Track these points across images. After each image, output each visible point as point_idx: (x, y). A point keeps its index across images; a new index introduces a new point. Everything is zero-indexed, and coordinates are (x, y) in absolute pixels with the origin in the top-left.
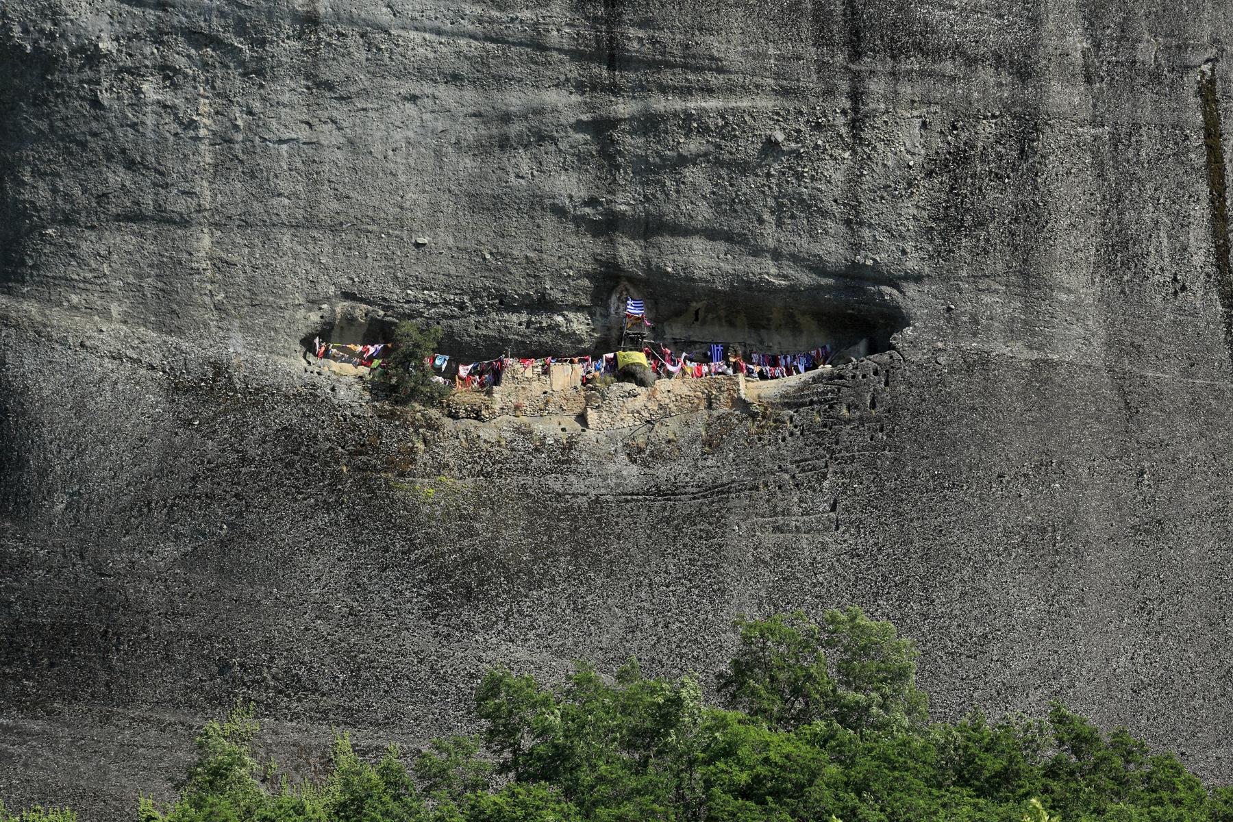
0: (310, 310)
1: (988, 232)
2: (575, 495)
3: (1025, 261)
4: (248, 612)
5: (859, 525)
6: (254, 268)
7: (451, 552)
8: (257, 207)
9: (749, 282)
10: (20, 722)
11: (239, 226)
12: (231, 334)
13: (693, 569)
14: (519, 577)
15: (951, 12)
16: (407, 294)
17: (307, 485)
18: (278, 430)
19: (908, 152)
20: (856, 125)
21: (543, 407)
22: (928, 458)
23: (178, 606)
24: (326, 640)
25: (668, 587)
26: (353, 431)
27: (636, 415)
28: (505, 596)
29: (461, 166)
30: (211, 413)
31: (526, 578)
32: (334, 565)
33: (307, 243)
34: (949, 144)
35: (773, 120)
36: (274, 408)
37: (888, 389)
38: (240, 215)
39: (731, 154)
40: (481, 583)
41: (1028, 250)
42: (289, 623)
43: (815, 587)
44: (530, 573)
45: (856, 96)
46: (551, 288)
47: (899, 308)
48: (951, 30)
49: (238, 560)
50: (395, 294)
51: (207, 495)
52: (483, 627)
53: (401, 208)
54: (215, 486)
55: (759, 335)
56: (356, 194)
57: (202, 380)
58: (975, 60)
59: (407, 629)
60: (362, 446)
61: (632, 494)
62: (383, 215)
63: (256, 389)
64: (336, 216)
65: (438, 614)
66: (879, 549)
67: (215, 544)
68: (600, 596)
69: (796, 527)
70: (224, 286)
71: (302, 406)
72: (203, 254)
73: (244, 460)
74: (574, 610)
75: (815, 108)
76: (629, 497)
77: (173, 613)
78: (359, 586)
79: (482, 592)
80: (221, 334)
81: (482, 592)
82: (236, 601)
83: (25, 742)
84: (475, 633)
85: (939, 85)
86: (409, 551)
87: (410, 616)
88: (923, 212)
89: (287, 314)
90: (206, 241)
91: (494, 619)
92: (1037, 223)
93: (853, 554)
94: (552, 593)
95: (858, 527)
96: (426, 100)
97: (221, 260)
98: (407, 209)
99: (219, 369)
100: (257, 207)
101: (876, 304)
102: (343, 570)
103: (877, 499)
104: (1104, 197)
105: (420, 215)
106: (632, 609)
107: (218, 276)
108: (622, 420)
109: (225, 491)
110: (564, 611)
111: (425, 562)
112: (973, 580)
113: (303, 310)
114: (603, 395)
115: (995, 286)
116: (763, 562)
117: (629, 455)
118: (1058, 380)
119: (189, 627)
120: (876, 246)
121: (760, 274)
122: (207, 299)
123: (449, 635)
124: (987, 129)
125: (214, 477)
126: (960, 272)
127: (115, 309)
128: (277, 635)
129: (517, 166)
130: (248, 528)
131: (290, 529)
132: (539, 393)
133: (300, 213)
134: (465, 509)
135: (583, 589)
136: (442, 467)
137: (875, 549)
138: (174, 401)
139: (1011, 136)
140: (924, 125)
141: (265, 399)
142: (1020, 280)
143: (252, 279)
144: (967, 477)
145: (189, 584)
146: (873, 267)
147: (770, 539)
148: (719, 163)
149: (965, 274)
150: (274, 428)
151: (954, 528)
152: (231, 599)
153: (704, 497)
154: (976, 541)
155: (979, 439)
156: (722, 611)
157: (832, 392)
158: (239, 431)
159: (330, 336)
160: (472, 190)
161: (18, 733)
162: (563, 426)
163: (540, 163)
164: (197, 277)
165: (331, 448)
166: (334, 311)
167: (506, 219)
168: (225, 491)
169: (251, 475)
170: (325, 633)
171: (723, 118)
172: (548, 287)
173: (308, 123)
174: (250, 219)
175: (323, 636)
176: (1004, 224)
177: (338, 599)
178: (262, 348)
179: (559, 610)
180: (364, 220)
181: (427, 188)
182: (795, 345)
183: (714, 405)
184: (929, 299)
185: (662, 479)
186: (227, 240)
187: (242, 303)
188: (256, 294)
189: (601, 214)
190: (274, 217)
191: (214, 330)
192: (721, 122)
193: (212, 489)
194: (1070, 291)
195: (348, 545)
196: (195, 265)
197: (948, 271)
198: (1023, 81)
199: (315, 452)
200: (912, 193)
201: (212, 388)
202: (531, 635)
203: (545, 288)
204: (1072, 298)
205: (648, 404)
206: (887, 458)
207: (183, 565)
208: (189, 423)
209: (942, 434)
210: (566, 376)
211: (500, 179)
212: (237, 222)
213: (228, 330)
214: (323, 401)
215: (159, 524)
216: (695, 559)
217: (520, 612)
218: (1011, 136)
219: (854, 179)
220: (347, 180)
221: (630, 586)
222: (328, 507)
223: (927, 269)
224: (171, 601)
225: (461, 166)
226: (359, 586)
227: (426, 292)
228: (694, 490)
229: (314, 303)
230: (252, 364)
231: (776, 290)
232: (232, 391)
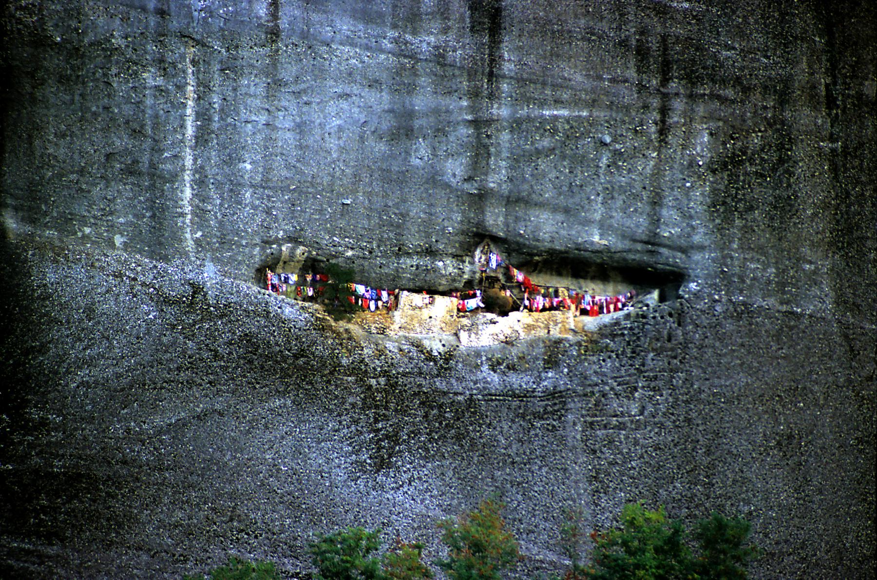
2: (456, 394)
10: (39, 548)
15: (733, 52)
16: (334, 241)
28: (408, 466)
30: (191, 321)
45: (664, 111)
48: (733, 66)
54: (194, 375)
55: (579, 283)
57: (184, 296)
58: (749, 89)
63: (225, 305)
73: (216, 356)
75: (634, 119)
76: (494, 398)
83: (43, 563)
85: (723, 107)
93: (657, 448)
96: (354, 98)
99: (197, 289)
101: (668, 265)
104: (837, 196)
112: (742, 472)
118: (802, 327)
124: (756, 140)
127: (118, 240)
133: (259, 178)
137: (672, 444)
138: (162, 310)
141: (231, 312)
146: (669, 238)
150: (238, 334)
153: (548, 400)
161: (37, 556)
162: (443, 342)
165: (280, 351)
171: (568, 123)
173: (267, 110)
189: (476, 189)
191: (193, 259)
192: (567, 127)
194: (811, 263)
202: (427, 496)
203: (432, 241)
204: (813, 267)
206: (680, 378)
210: (444, 305)
215: (151, 402)
217: (420, 479)
227: (347, 240)
228: (540, 394)
230: (221, 286)
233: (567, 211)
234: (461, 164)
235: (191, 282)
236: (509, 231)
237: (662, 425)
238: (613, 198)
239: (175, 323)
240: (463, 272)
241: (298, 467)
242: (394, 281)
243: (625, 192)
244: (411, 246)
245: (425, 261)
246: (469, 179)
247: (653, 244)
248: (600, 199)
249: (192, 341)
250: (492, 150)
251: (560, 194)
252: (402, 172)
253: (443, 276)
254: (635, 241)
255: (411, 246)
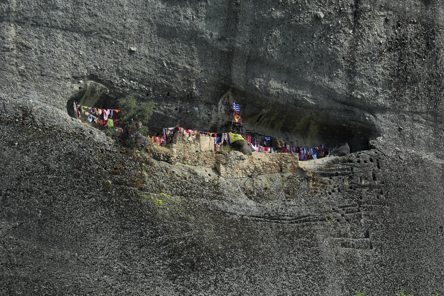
0: (73, 82)
1: (418, 87)
3: (435, 106)
4: (61, 267)
5: (381, 246)
6: (42, 52)
7: (180, 240)
8: (44, 14)
9: (296, 100)
11: (32, 25)
12: (30, 91)
13: (307, 264)
14: (219, 259)
16: (123, 81)
17: (90, 189)
18: (66, 154)
19: (378, 35)
20: (356, 15)
21: (196, 160)
22: (406, 212)
23: (14, 260)
24: (111, 288)
25: (296, 273)
26: (108, 159)
27: (244, 171)
29: (157, 6)
31: (223, 260)
32: (111, 242)
33: (72, 41)
34: (396, 34)
35: (318, 5)
36: (62, 140)
37: (380, 170)
38: (33, 18)
39: (296, 21)
40: (198, 260)
41: (437, 101)
42: (88, 275)
43: (367, 281)
44: (224, 257)
46: (196, 89)
47: (374, 125)
49: (51, 233)
50: (117, 80)
51: (27, 190)
52: (203, 288)
53: (124, 27)
54: (32, 185)
56: (101, 14)
57: (16, 118)
59: (159, 285)
60: (115, 169)
61: (257, 217)
62: (114, 30)
64: (89, 26)
65: (176, 278)
66: (392, 263)
67: (35, 222)
68: (262, 275)
69: (353, 245)
70: (25, 60)
71: (77, 140)
72: (10, 39)
73: (48, 170)
74: (250, 282)
77: (11, 264)
78: (127, 256)
79: (200, 266)
80: (24, 90)
81: (200, 266)
82: (52, 259)
84: (199, 291)
86: (155, 237)
87: (159, 277)
88: (387, 71)
89: (62, 83)
90: (13, 32)
91: (209, 283)
92: (440, 85)
94: (238, 270)
95: (381, 248)
97: (22, 44)
98: (127, 28)
100: (44, 14)
101: (360, 122)
102: (115, 245)
103: (387, 233)
105: (133, 33)
106: (280, 285)
107: (21, 54)
108: (237, 173)
109: (39, 189)
110: (245, 282)
111: (165, 244)
113: (70, 82)
114: (226, 156)
115: (421, 119)
116: (341, 263)
117: (246, 194)
119: (23, 274)
120: (362, 88)
121: (303, 96)
122: (14, 68)
123: (184, 291)
125: (31, 179)
126: (405, 108)
128: (81, 283)
129: (185, 11)
130: (56, 213)
131: (83, 216)
132: (194, 151)
133: (68, 21)
134: (181, 214)
135: (253, 270)
136: (160, 188)
137: (390, 262)
139: (421, 35)
140: (386, 20)
142: (433, 118)
143: (41, 59)
144: (426, 226)
145: (20, 246)
146: (361, 100)
147: (343, 250)
148: (290, 26)
149: (407, 110)
151: (423, 255)
152: (49, 258)
153: (296, 222)
154: (434, 264)
155: (428, 205)
156: (325, 291)
157: (348, 169)
158: (43, 151)
159: (80, 101)
160: (160, 22)
163: (197, 11)
164: (7, 53)
165: (99, 168)
166: (87, 85)
167: (176, 44)
168: (39, 189)
169: (55, 180)
170: (110, 284)
172: (194, 88)
174: (39, 22)
175: (110, 286)
176: (425, 83)
177: (115, 263)
178: (49, 102)
179: (242, 281)
180: (104, 31)
181: (138, 17)
182: (305, 143)
183: (284, 171)
184: (389, 122)
185: (270, 210)
186: (25, 33)
187: (35, 73)
188: (43, 68)
189: (226, 47)
190: (53, 22)
191: (20, 87)
193: (31, 187)
195: (118, 229)
196: (7, 46)
197: (399, 107)
198: (426, 5)
199: (90, 169)
200: (382, 59)
201: (23, 123)
205: (250, 165)
207: (14, 233)
208: (11, 144)
209: (411, 200)
211: (175, 18)
212: (31, 22)
213: (28, 88)
214: (89, 139)
216: (306, 258)
217: (222, 280)
218: (421, 35)
219: (353, 47)
220: (96, 5)
221: (276, 270)
222: (104, 205)
223: (388, 104)
224: (9, 256)
225: (157, 6)
226: (127, 256)
228: (290, 218)
229: (76, 78)
230: (45, 111)
231: (309, 107)
232: (36, 126)
233: (289, 72)
234: (216, 26)
235: (20, 106)
236: (248, 85)
237: (382, 245)
238: (322, 64)
239: (12, 140)
240: (211, 118)
241: (126, 267)
242: (163, 120)
243: (331, 60)
244: (177, 92)
245: (185, 106)
246: (221, 39)
247: (349, 105)
248: (313, 63)
249: (28, 155)
250: (240, 16)
251: (285, 58)
252: (174, 28)
253: (198, 120)
254: (336, 101)
255: (177, 92)
